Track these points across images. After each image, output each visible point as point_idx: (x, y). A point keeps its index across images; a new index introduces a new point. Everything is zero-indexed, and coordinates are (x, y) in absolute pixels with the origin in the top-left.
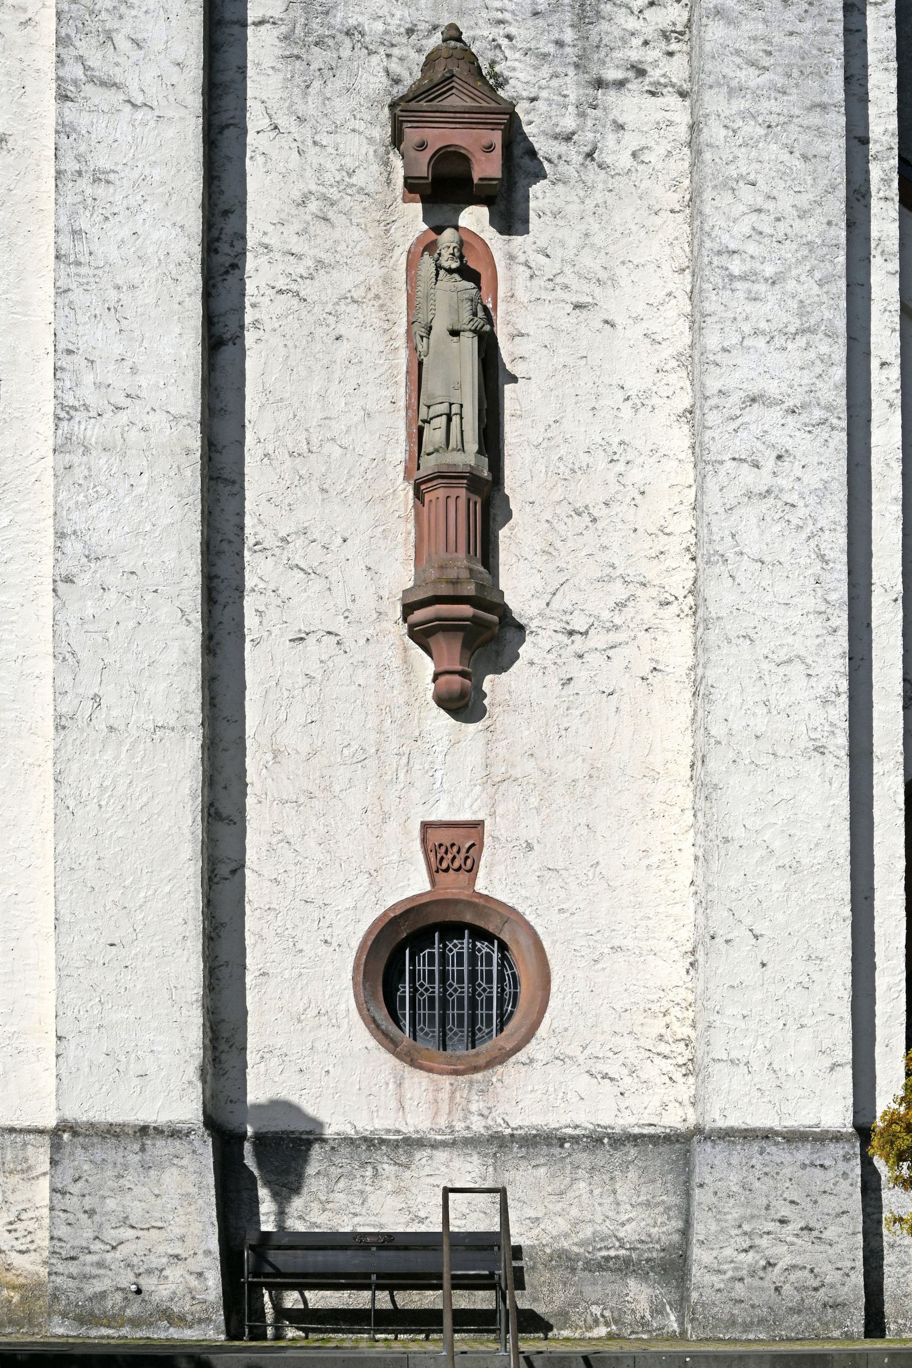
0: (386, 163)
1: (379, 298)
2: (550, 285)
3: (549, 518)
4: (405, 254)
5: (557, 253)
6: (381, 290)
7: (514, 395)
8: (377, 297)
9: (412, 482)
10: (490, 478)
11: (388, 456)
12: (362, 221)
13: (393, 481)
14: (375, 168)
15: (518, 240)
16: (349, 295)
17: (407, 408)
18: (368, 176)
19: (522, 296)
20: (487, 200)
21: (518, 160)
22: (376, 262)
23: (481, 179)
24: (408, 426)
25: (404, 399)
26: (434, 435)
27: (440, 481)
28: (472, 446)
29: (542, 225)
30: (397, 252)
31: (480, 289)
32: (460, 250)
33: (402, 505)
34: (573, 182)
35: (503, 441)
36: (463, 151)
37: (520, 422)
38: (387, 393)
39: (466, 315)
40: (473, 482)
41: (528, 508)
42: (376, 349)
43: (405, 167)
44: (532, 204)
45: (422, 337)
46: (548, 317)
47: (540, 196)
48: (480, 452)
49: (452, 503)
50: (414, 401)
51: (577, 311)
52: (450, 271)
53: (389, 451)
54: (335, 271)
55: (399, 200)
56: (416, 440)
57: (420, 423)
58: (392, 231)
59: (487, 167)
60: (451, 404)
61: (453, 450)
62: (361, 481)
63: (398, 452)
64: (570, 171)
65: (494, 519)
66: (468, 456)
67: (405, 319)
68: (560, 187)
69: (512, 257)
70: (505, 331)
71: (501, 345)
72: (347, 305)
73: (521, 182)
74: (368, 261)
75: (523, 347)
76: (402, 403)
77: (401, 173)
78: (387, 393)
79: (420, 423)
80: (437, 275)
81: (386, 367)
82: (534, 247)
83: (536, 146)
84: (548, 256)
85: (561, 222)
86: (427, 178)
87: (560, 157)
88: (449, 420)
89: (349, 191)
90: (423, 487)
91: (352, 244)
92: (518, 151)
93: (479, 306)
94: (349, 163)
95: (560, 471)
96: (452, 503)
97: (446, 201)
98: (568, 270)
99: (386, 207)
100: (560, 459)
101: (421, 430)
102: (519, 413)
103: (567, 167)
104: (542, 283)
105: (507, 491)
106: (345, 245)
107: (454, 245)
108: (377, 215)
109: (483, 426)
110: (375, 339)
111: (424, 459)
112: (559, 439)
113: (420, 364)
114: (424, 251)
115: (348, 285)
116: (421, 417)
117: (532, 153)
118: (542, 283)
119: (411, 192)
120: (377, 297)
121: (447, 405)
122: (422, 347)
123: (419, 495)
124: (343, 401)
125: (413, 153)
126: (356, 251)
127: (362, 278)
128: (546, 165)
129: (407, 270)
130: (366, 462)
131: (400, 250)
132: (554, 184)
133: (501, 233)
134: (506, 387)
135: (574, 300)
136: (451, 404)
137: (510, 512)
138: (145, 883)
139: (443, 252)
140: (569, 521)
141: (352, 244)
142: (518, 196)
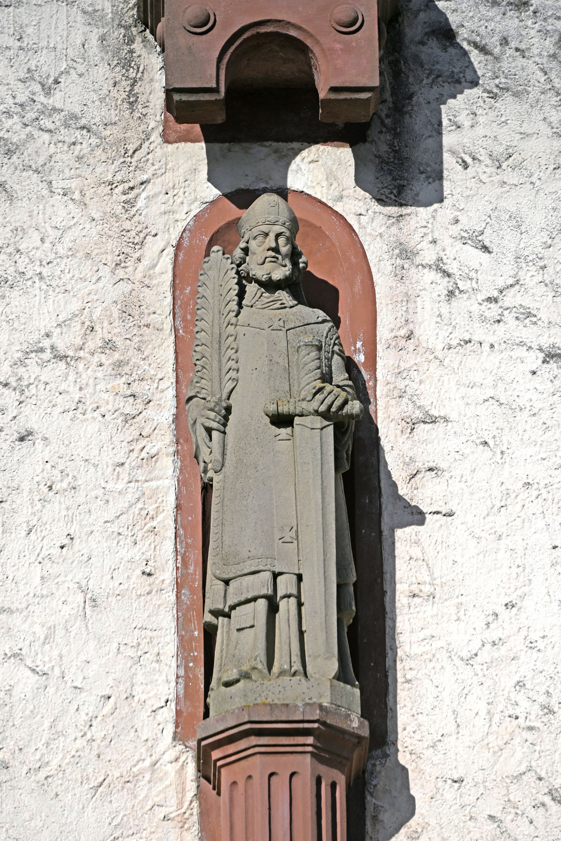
0: (127, 63)
1: (114, 348)
2: (493, 311)
3: (496, 812)
4: (170, 251)
5: (506, 241)
6: (116, 331)
7: (416, 552)
8: (109, 345)
9: (193, 743)
10: (365, 732)
11: (138, 690)
12: (74, 184)
13: (150, 744)
14: (102, 74)
15: (420, 215)
16: (46, 343)
17: (179, 586)
18: (90, 88)
19: (430, 333)
20: (352, 134)
21: (413, 49)
22: (105, 271)
23: (334, 90)
24: (182, 623)
25: (171, 565)
26: (240, 643)
27: (253, 740)
28: (325, 660)
29: (472, 183)
30: (153, 247)
31: (337, 322)
32: (291, 240)
33: (172, 792)
34: (534, 93)
35: (394, 650)
36: (293, 33)
37: (429, 609)
38: (136, 553)
39: (309, 381)
40: (329, 742)
41: (450, 793)
42: (109, 458)
43: (166, 67)
44: (449, 139)
45: (209, 431)
46: (489, 381)
47: (466, 124)
48: (342, 676)
49: (280, 785)
50: (195, 569)
51: (553, 365)
52: (270, 286)
53: (140, 678)
54: (15, 293)
55: (156, 137)
56: (199, 654)
57: (209, 618)
58: (141, 203)
59: (347, 65)
60: (276, 576)
61: (282, 673)
62: (80, 743)
63: (161, 678)
64: (530, 70)
65: (375, 818)
66: (317, 686)
67: (171, 392)
68: (507, 104)
69: (406, 253)
70: (395, 412)
71: (385, 443)
72: (43, 364)
73: (423, 94)
74: (87, 268)
75: (431, 446)
76: (167, 575)
77: (159, 81)
78: (136, 553)
79: (209, 618)
80: (241, 294)
81: (130, 497)
82: (455, 230)
83: (454, 20)
84: (485, 249)
85: (512, 178)
86: (215, 90)
87: (505, 41)
88: (273, 608)
89: (47, 123)
90: (216, 754)
91: (53, 234)
92: (413, 30)
93: (337, 361)
94: (46, 64)
95: (518, 711)
96: (280, 785)
97: (261, 137)
98: (531, 276)
99: (128, 154)
100: (520, 684)
101: (210, 634)
102: (427, 589)
103: (521, 61)
104: (475, 308)
105: (403, 759)
106: (36, 236)
107: (278, 229)
108: (107, 172)
109: (348, 621)
110: (105, 436)
111: (217, 691)
112: (517, 643)
113: (207, 488)
114: (211, 243)
115: (46, 322)
116: (209, 605)
117: (446, 34)
118: (475, 308)
119: (179, 120)
120: (109, 345)
121: (268, 576)
122: (209, 453)
123: (207, 771)
124: (37, 571)
125: (184, 39)
126: (61, 249)
127: (75, 306)
128: (475, 56)
129: (174, 286)
130: (89, 702)
131: (160, 242)
132: (495, 97)
133: (380, 201)
134: (399, 533)
135: (545, 342)
136: (276, 576)
137: (412, 800)
138: (155, 824)
139: (253, 245)
140: (539, 815)
141: (53, 234)
142: (418, 122)
